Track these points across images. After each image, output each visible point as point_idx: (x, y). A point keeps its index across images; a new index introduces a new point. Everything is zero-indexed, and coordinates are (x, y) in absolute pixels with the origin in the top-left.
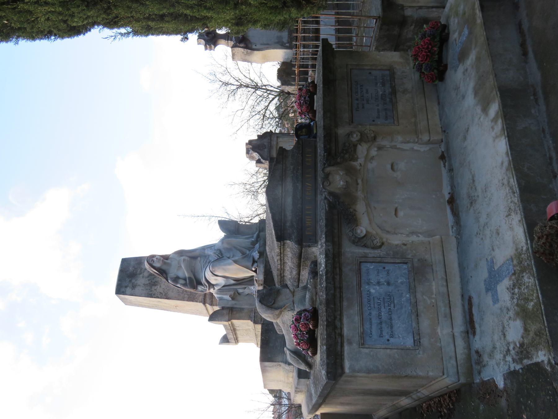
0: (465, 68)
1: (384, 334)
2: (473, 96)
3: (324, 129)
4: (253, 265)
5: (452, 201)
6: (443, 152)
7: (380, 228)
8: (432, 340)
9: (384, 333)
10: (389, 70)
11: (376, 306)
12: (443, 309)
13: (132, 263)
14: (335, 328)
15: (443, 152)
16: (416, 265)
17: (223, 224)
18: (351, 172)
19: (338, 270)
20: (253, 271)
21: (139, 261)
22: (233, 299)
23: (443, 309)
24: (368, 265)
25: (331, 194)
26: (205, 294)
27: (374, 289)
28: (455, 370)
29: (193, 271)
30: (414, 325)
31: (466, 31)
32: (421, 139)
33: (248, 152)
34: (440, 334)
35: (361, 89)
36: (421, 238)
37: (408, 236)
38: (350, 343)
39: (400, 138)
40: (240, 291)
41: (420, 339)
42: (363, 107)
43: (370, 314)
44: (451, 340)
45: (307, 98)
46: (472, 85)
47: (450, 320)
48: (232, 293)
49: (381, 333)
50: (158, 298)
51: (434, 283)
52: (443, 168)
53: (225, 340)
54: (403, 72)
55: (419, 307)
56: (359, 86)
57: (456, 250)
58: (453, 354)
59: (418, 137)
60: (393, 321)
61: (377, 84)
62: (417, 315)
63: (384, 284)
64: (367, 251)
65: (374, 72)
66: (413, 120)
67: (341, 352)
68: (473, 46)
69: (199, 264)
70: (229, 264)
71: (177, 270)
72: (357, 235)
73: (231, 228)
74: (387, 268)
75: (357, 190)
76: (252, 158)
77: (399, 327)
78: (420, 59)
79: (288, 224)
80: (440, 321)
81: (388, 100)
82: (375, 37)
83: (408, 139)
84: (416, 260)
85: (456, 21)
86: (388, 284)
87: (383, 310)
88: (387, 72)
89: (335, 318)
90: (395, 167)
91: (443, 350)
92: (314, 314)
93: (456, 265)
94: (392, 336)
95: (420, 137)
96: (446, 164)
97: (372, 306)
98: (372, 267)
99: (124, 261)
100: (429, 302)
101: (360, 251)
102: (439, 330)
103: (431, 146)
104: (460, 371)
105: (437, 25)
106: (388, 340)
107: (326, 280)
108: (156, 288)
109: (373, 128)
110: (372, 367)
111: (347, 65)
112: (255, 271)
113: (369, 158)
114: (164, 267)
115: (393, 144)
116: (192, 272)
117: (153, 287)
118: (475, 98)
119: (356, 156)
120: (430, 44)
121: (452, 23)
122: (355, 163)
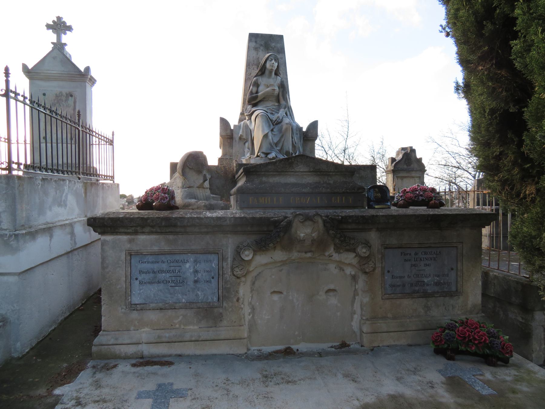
0: (436, 386)
1: (143, 275)
2: (392, 393)
3: (373, 216)
4: (263, 153)
5: (288, 352)
6: (349, 346)
7: (258, 275)
8: (136, 323)
9: (143, 276)
10: (457, 291)
11: (172, 268)
12: (167, 335)
14: (143, 227)
15: (349, 346)
16: (216, 310)
17: (314, 126)
18: (319, 245)
19: (205, 230)
21: (282, 50)
22: (240, 138)
23: (167, 335)
24: (216, 262)
25: (289, 224)
27: (190, 267)
28: (104, 343)
29: (264, 99)
30: (152, 305)
31: (486, 391)
32: (365, 323)
33: (403, 149)
34: (143, 330)
35: (431, 259)
36: (248, 318)
37: (250, 303)
38: (130, 241)
39: (366, 300)
40: (247, 144)
41: (137, 310)
42: (406, 260)
43: (163, 262)
44: (134, 341)
45: (421, 198)
46: (408, 392)
47: (155, 341)
48: (244, 137)
49: (143, 273)
51: (196, 327)
52: (330, 344)
54: (453, 307)
55: (170, 311)
56: (435, 256)
57: (231, 352)
58: (120, 342)
59: (367, 320)
60: (156, 285)
61: (438, 276)
62: (161, 309)
63: (195, 277)
64: (230, 260)
65: (453, 274)
66: (390, 315)
67: (120, 233)
68: (460, 400)
69: (271, 104)
70: (263, 130)
71: (265, 85)
72: (242, 250)
73: (310, 135)
74: (212, 280)
75: (299, 252)
76: (398, 153)
77: (151, 290)
78: (461, 328)
79: (264, 179)
80: (156, 331)
81: (417, 288)
82: (509, 276)
83: (365, 308)
84: (221, 310)
85: (508, 378)
86: (196, 282)
87: (168, 275)
88: (454, 289)
89: (152, 227)
90: (331, 294)
91: (126, 332)
92: (172, 207)
93: (214, 351)
94: (141, 283)
95: (367, 322)
96: (333, 349)
97: (172, 265)
98: (213, 265)
99: (281, 38)
100: (176, 321)
101: (229, 254)
102: (146, 329)
103: (358, 334)
104: (103, 347)
105: (508, 353)
106: (137, 279)
107: (191, 218)
109: (378, 271)
110: (107, 262)
111: (462, 243)
112: (258, 156)
113: (341, 266)
114: (267, 72)
115: (360, 293)
116: (264, 98)
117: (256, 67)
118: (389, 395)
119: (341, 251)
120: (480, 343)
121: (507, 371)
122: (332, 249)
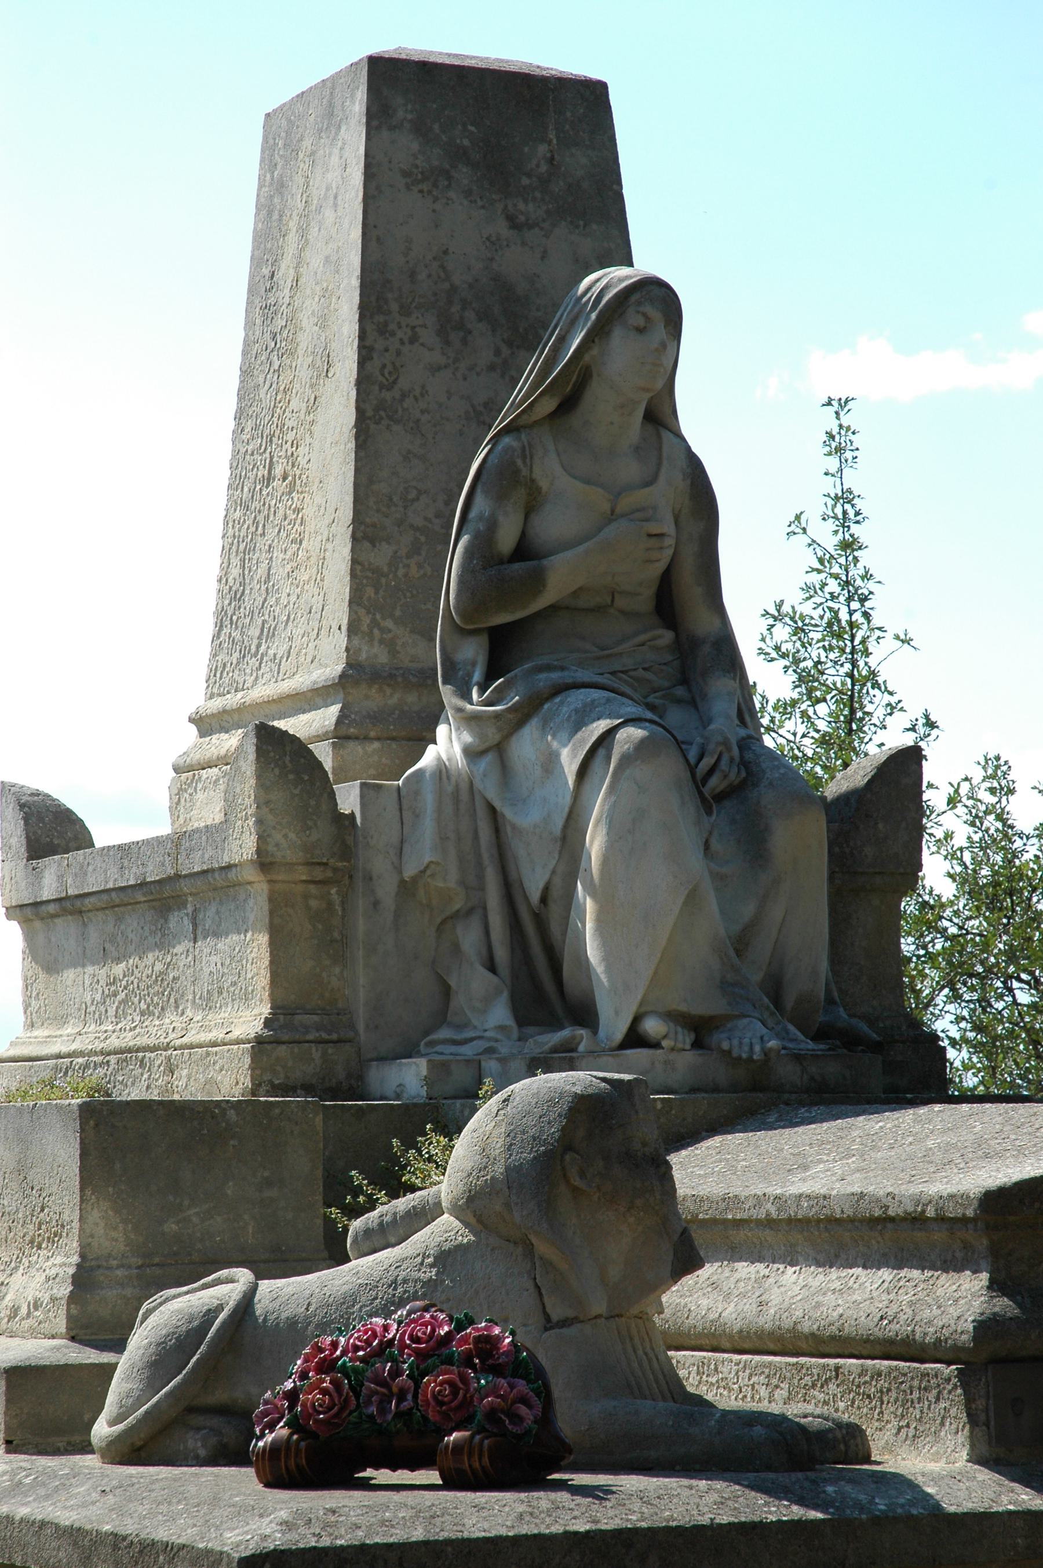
13: (578, 162)
20: (637, 1020)
26: (426, 679)
50: (362, 362)
53: (51, 830)
99: (588, 101)
108: (428, 336)
112: (635, 1039)
